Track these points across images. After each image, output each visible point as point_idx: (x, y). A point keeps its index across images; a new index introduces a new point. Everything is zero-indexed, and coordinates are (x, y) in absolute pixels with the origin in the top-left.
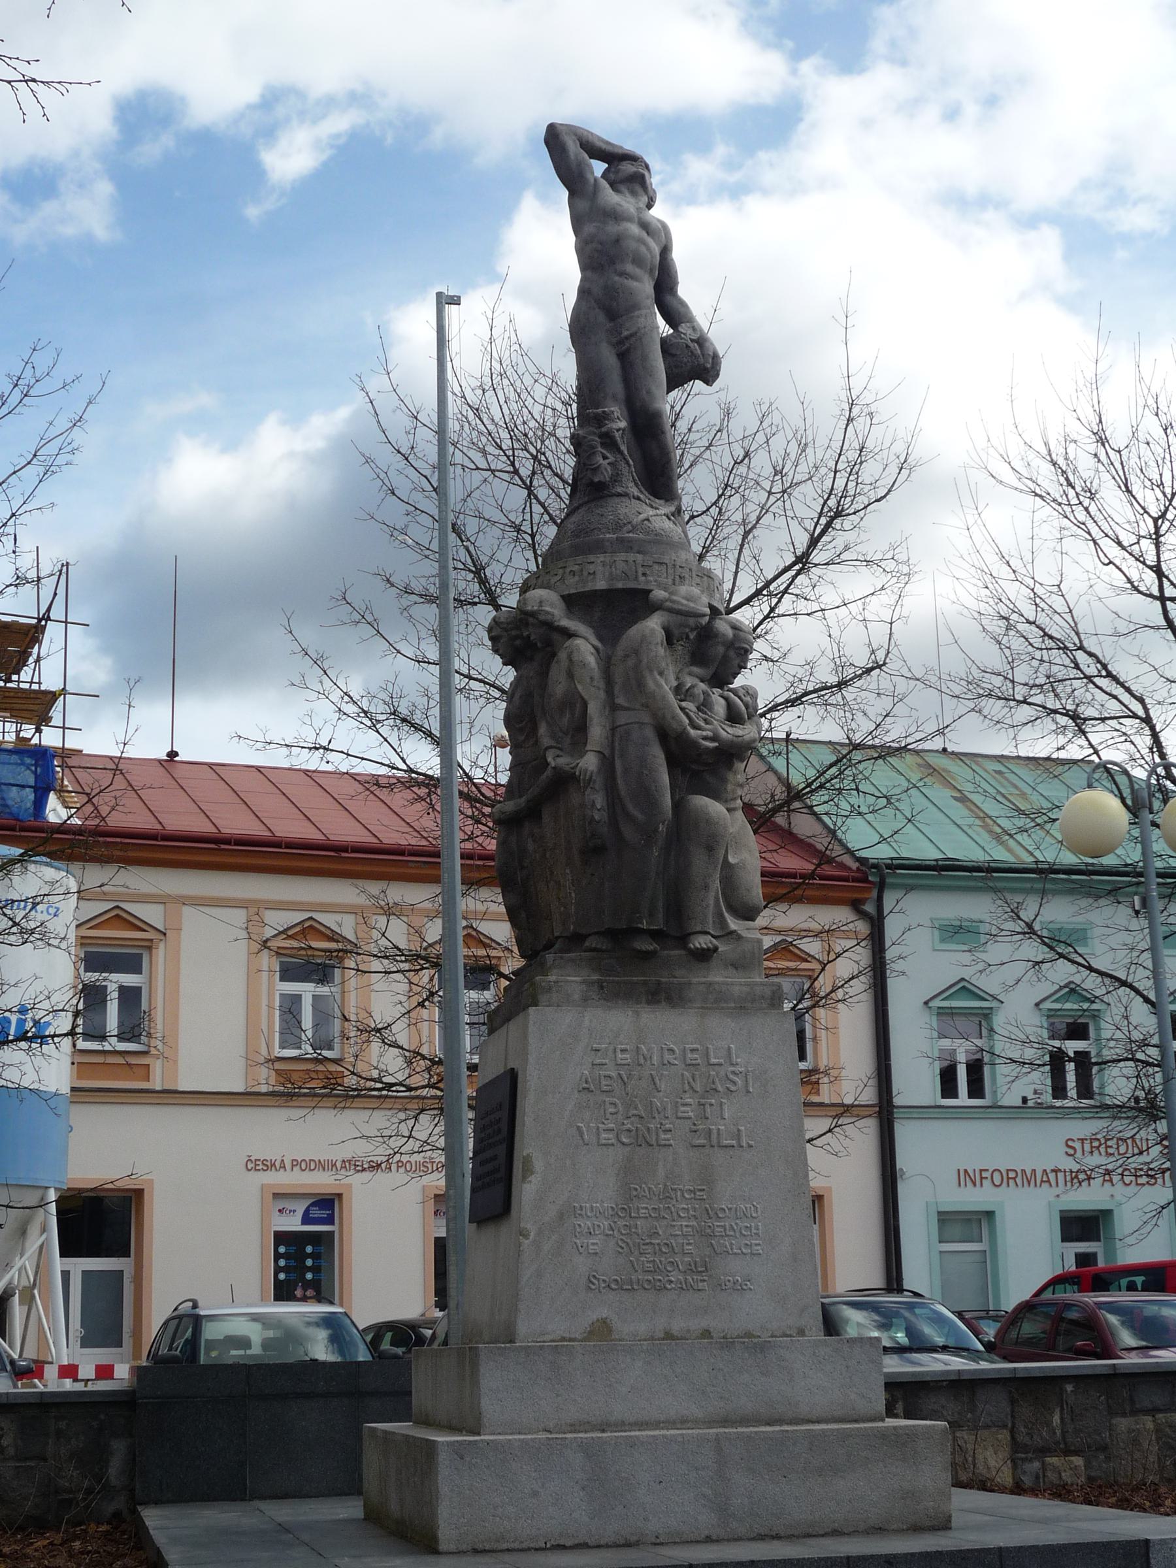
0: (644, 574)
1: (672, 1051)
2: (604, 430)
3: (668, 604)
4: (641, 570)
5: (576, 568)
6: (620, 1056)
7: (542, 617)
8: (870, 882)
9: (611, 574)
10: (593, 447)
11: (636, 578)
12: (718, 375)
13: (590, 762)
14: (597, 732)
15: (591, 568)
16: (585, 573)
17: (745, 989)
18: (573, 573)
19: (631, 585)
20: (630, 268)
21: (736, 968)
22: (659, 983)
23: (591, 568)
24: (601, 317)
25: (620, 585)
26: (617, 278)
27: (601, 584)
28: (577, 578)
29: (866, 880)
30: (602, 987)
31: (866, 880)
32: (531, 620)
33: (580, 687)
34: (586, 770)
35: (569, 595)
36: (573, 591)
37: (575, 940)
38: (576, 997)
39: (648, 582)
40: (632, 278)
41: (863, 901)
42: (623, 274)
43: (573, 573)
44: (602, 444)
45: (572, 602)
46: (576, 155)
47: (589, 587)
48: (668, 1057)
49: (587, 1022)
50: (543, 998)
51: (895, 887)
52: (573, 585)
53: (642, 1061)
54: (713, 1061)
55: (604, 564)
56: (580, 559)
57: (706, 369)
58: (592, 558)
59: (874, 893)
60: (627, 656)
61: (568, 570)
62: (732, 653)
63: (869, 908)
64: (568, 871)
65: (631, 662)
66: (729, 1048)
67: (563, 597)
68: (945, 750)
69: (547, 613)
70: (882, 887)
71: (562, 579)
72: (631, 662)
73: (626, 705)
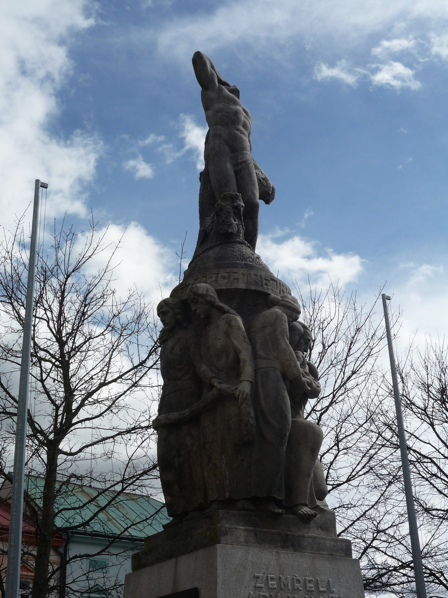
0: (266, 284)
1: (298, 581)
2: (235, 204)
3: (282, 302)
4: (264, 282)
5: (225, 275)
6: (271, 583)
7: (208, 299)
8: (63, 539)
9: (248, 281)
10: (229, 213)
11: (262, 286)
12: (274, 199)
13: (245, 387)
14: (248, 370)
15: (236, 276)
16: (232, 279)
17: (332, 543)
18: (224, 278)
19: (260, 289)
20: (241, 128)
21: (323, 530)
22: (287, 535)
23: (236, 276)
24: (227, 149)
25: (253, 288)
26: (236, 132)
27: (242, 286)
28: (226, 280)
29: (61, 538)
30: (256, 535)
31: (61, 538)
32: (200, 299)
33: (236, 342)
34: (244, 392)
35: (221, 290)
36: (223, 287)
37: (229, 503)
38: (242, 539)
39: (268, 289)
40: (243, 134)
41: (59, 547)
42: (238, 130)
43: (224, 278)
44: (234, 212)
45: (220, 292)
46: (211, 70)
47: (234, 286)
48: (297, 585)
49: (250, 558)
50: (223, 539)
51: (74, 542)
52: (223, 284)
53: (283, 586)
54: (321, 589)
55: (243, 275)
56: (228, 270)
57: (269, 194)
58: (236, 270)
59: (64, 544)
60: (264, 327)
61: (220, 275)
62: (302, 341)
63: (61, 550)
64: (223, 457)
65: (268, 330)
66: (329, 581)
67: (216, 290)
68: (90, 486)
69: (211, 296)
70: (68, 542)
71: (216, 281)
72: (268, 330)
73: (264, 355)
